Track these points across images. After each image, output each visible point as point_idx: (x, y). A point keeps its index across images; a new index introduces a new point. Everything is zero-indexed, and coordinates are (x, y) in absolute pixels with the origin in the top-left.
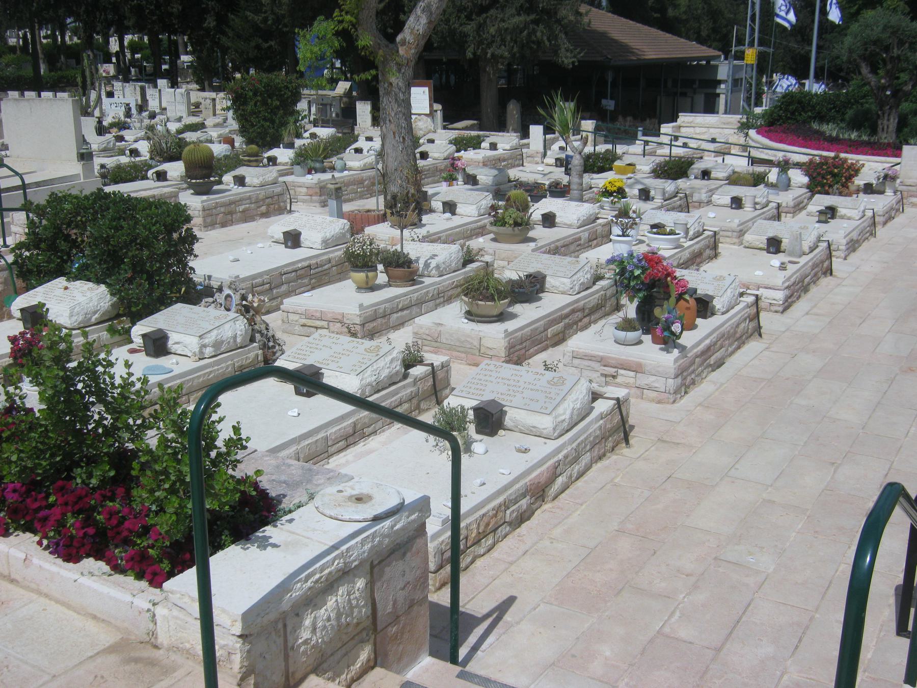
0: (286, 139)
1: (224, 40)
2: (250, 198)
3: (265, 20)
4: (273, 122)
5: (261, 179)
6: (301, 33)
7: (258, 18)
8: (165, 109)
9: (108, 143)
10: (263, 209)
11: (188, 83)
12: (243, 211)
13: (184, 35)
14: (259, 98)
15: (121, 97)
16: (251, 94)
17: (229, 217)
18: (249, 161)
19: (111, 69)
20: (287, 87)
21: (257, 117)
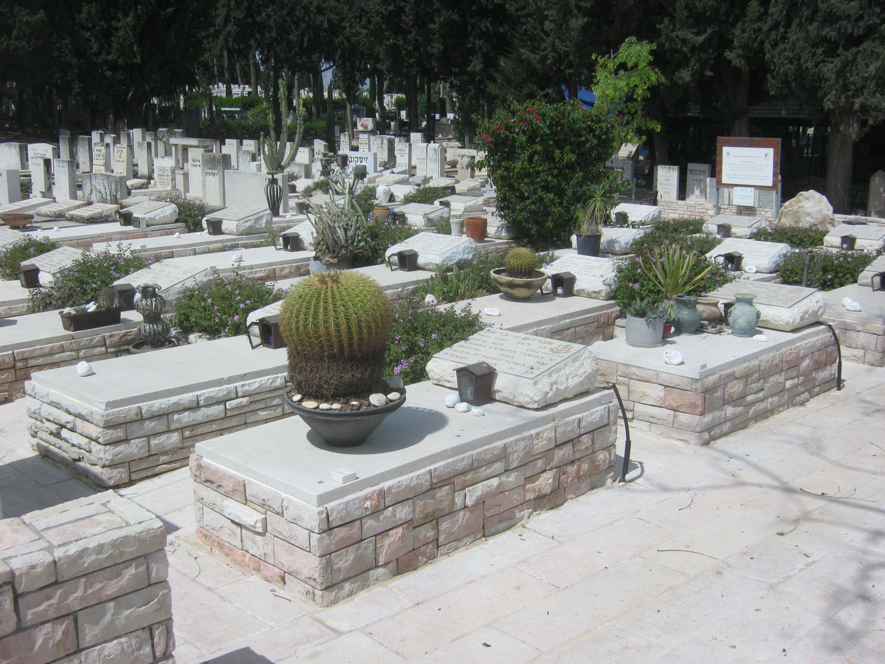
0: (585, 227)
1: (491, 88)
2: (504, 455)
3: (544, 59)
4: (561, 193)
5: (544, 385)
6: (601, 61)
7: (534, 58)
8: (415, 167)
9: (258, 219)
10: (545, 482)
11: (449, 140)
12: (481, 502)
13: (446, 82)
14: (538, 147)
15: (366, 151)
16: (524, 139)
17: (427, 532)
18: (512, 285)
19: (369, 123)
20: (591, 130)
21: (533, 183)
